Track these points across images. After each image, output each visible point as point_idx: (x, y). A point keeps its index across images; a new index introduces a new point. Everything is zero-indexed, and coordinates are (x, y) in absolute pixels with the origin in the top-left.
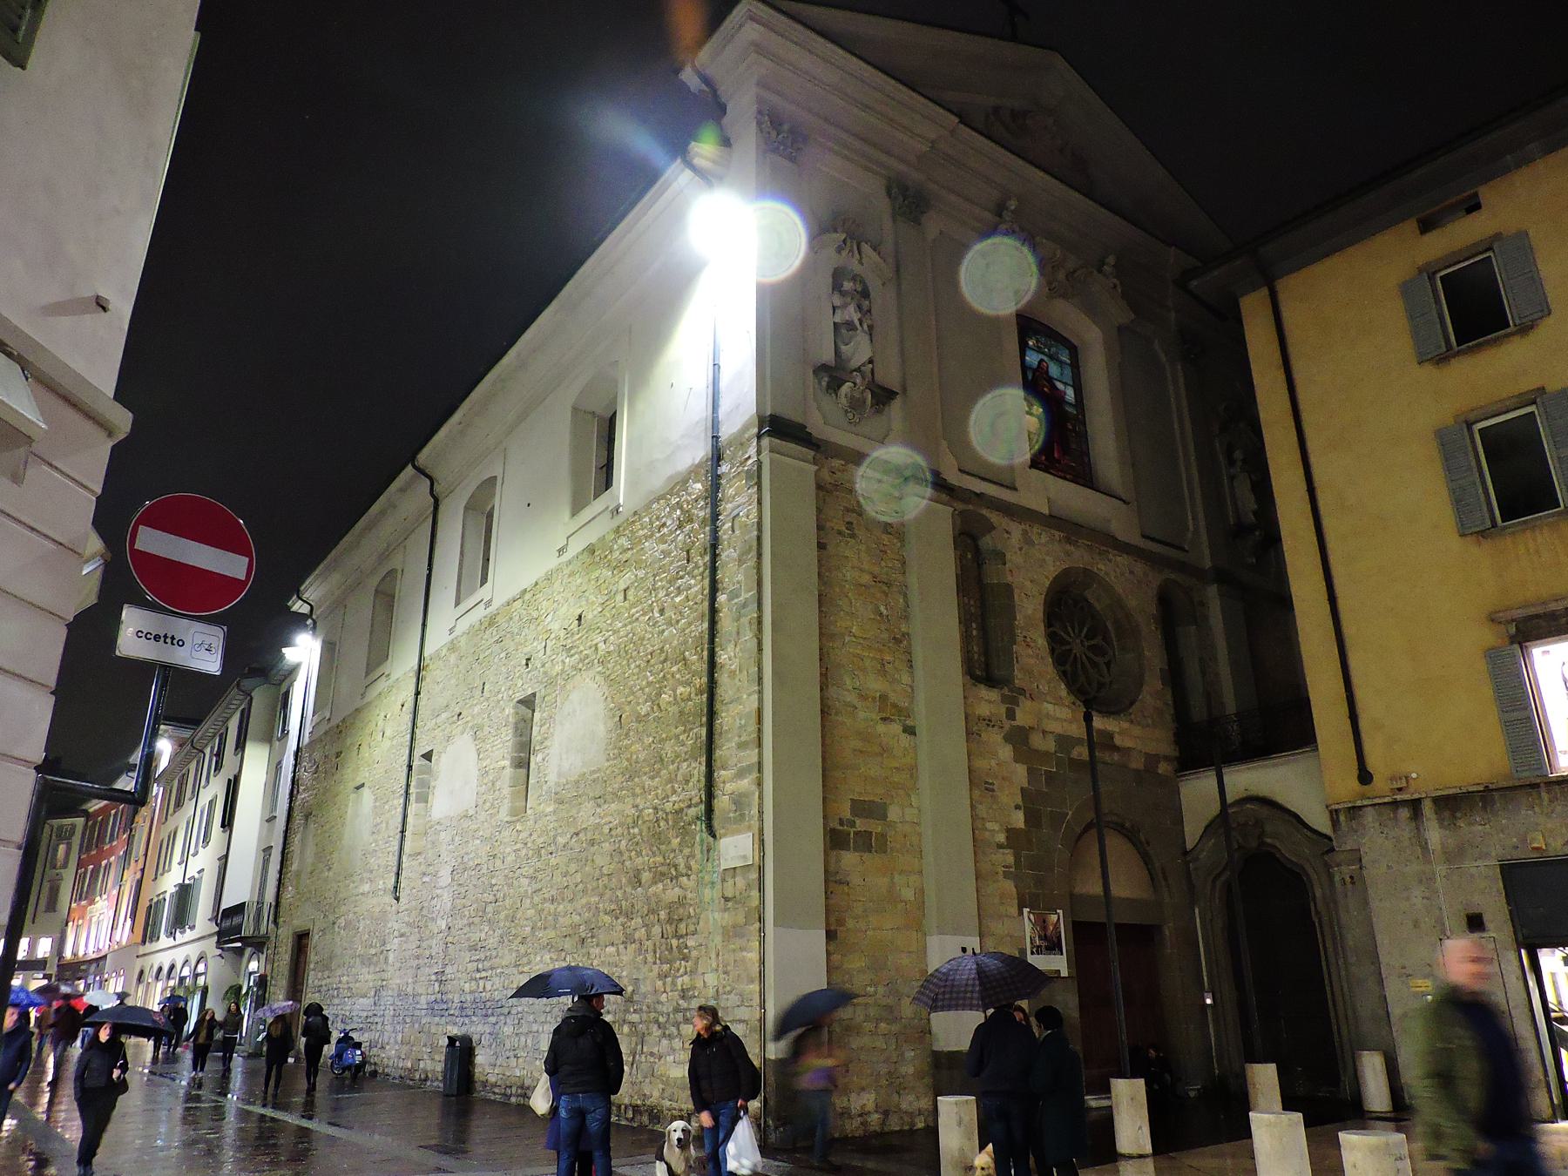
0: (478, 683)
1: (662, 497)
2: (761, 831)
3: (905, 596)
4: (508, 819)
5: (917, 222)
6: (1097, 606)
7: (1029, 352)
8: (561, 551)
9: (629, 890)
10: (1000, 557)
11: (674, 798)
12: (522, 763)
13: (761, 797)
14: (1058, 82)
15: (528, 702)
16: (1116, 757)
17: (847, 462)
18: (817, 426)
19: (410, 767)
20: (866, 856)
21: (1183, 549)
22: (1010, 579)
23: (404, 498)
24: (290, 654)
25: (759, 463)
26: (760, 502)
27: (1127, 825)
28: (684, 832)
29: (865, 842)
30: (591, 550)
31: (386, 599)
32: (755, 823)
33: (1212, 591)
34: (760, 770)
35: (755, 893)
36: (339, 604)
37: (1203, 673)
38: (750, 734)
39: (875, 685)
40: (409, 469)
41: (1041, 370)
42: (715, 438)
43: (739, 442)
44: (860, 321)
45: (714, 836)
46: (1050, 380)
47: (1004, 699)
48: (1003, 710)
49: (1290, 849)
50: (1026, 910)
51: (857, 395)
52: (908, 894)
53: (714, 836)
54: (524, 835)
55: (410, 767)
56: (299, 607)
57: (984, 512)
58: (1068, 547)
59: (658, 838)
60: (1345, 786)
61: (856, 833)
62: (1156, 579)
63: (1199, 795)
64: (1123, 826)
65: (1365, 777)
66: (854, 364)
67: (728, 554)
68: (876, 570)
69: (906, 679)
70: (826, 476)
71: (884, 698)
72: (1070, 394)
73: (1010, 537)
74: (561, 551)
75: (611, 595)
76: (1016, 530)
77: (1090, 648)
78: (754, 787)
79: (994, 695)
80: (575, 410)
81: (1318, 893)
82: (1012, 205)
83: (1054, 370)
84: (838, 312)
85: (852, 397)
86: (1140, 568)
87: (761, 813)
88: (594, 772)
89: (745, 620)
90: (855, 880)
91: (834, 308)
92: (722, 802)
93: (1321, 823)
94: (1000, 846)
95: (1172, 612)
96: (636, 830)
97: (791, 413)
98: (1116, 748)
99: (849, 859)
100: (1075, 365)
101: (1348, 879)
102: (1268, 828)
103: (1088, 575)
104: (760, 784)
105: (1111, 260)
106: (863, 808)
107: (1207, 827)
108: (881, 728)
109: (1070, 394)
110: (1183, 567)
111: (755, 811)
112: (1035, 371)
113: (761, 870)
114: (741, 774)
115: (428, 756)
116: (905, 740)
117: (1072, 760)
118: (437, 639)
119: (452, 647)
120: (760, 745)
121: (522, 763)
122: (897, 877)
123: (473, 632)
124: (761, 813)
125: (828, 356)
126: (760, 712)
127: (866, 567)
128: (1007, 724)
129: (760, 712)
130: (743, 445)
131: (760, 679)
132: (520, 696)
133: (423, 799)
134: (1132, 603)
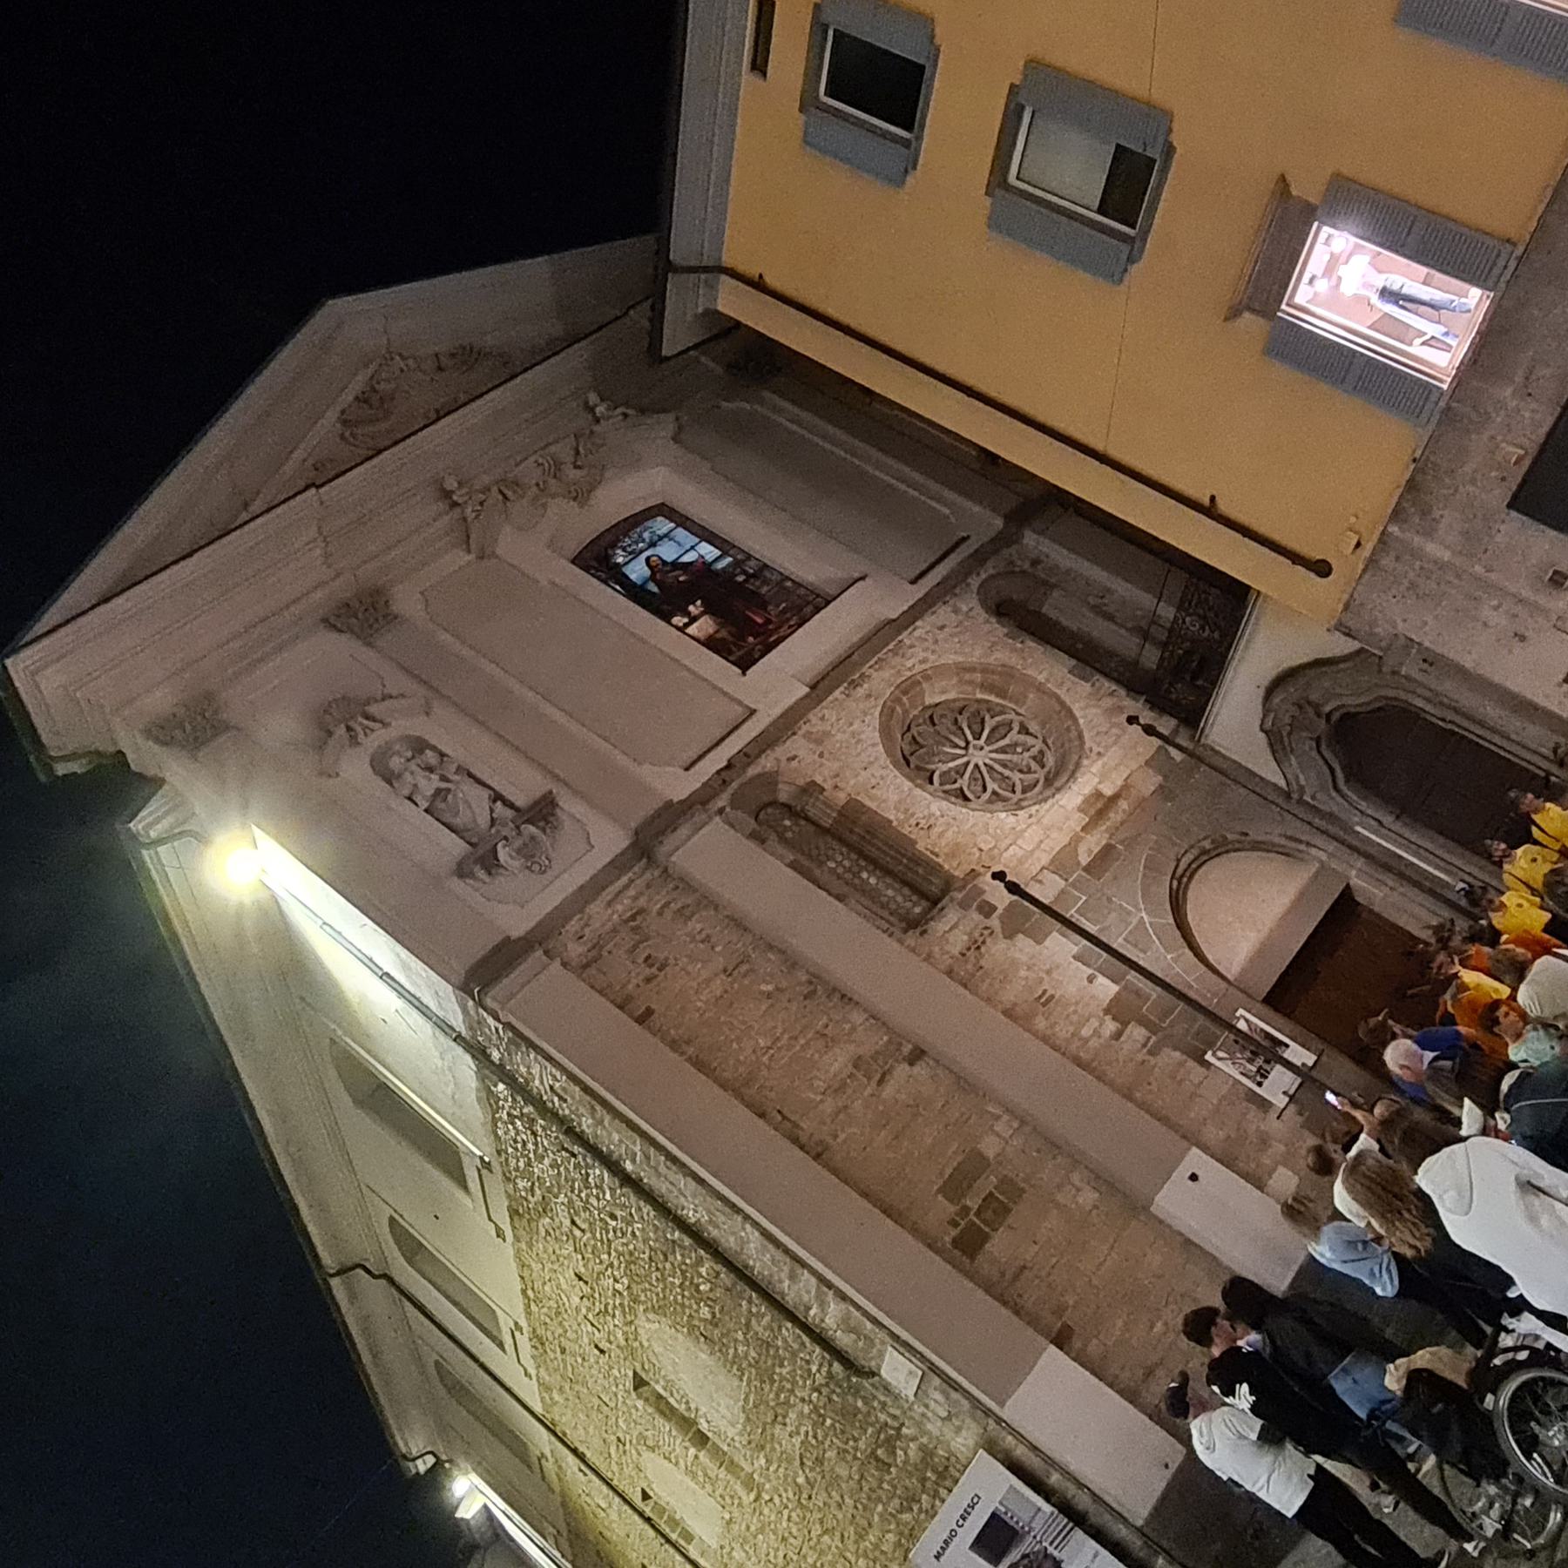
0: (596, 1401)
1: (494, 1121)
2: (895, 1337)
3: (771, 947)
4: (752, 1496)
5: (392, 618)
6: (952, 695)
7: (627, 570)
8: (500, 1234)
9: (887, 1478)
10: (812, 789)
11: (814, 1369)
12: (701, 1440)
13: (858, 1308)
14: (360, 326)
15: (639, 1383)
16: (1123, 805)
17: (581, 911)
18: (518, 924)
19: (648, 1520)
20: (1010, 1220)
21: (964, 539)
22: (841, 798)
23: (361, 1308)
24: (467, 1511)
25: (508, 1026)
26: (549, 1058)
27: (1207, 844)
28: (856, 1391)
29: (997, 1209)
30: (514, 1213)
31: (458, 1390)
32: (882, 1335)
33: (1030, 539)
34: (830, 1286)
35: (955, 1395)
36: (443, 1428)
37: (1110, 618)
38: (786, 1265)
39: (837, 1062)
40: (335, 1283)
41: (659, 569)
42: (458, 1039)
43: (476, 1025)
44: (444, 778)
45: (873, 1374)
46: (675, 565)
47: (964, 905)
48: (976, 916)
49: (1351, 695)
50: (1209, 1057)
51: (518, 843)
52: (1088, 1197)
53: (873, 1374)
54: (777, 1500)
55: (648, 1520)
56: (422, 1466)
57: (752, 771)
58: (860, 691)
59: (848, 1414)
60: (1326, 593)
61: (978, 1214)
62: (969, 603)
63: (1235, 717)
64: (1204, 852)
65: (1322, 569)
66: (483, 821)
67: (586, 1124)
68: (720, 962)
69: (858, 1017)
70: (575, 950)
71: (857, 1063)
72: (708, 551)
73: (799, 760)
74: (500, 1234)
75: (570, 1235)
76: (796, 745)
77: (989, 741)
78: (843, 1306)
79: (952, 915)
80: (358, 1103)
81: (1420, 703)
82: (450, 484)
83: (667, 552)
84: (418, 799)
85: (519, 851)
86: (943, 614)
87: (875, 1321)
88: (746, 1400)
89: (662, 1169)
90: (1029, 1253)
91: (410, 799)
92: (843, 1340)
93: (1342, 646)
94: (1118, 1035)
95: (1021, 615)
96: (829, 1422)
97: (480, 947)
98: (1114, 798)
99: (999, 1245)
100: (683, 521)
101: (1425, 666)
102: (1314, 697)
103: (909, 687)
104: (843, 1297)
105: (593, 398)
106: (955, 1187)
107: (1274, 752)
108: (888, 1091)
109: (708, 551)
110: (979, 558)
111: (869, 1325)
112: (652, 578)
113: (933, 1368)
114: (823, 1305)
115: (645, 1496)
116: (920, 1070)
117: (1087, 869)
118: (530, 1392)
119: (545, 1387)
120: (804, 1265)
121: (701, 1440)
122: (1060, 1197)
123: (540, 1360)
124: (875, 1321)
125: (456, 847)
126: (766, 1234)
127: (705, 974)
128: (994, 922)
129: (766, 1234)
130: (481, 1022)
131: (733, 1206)
132: (629, 1384)
133: (689, 1537)
134: (976, 655)
